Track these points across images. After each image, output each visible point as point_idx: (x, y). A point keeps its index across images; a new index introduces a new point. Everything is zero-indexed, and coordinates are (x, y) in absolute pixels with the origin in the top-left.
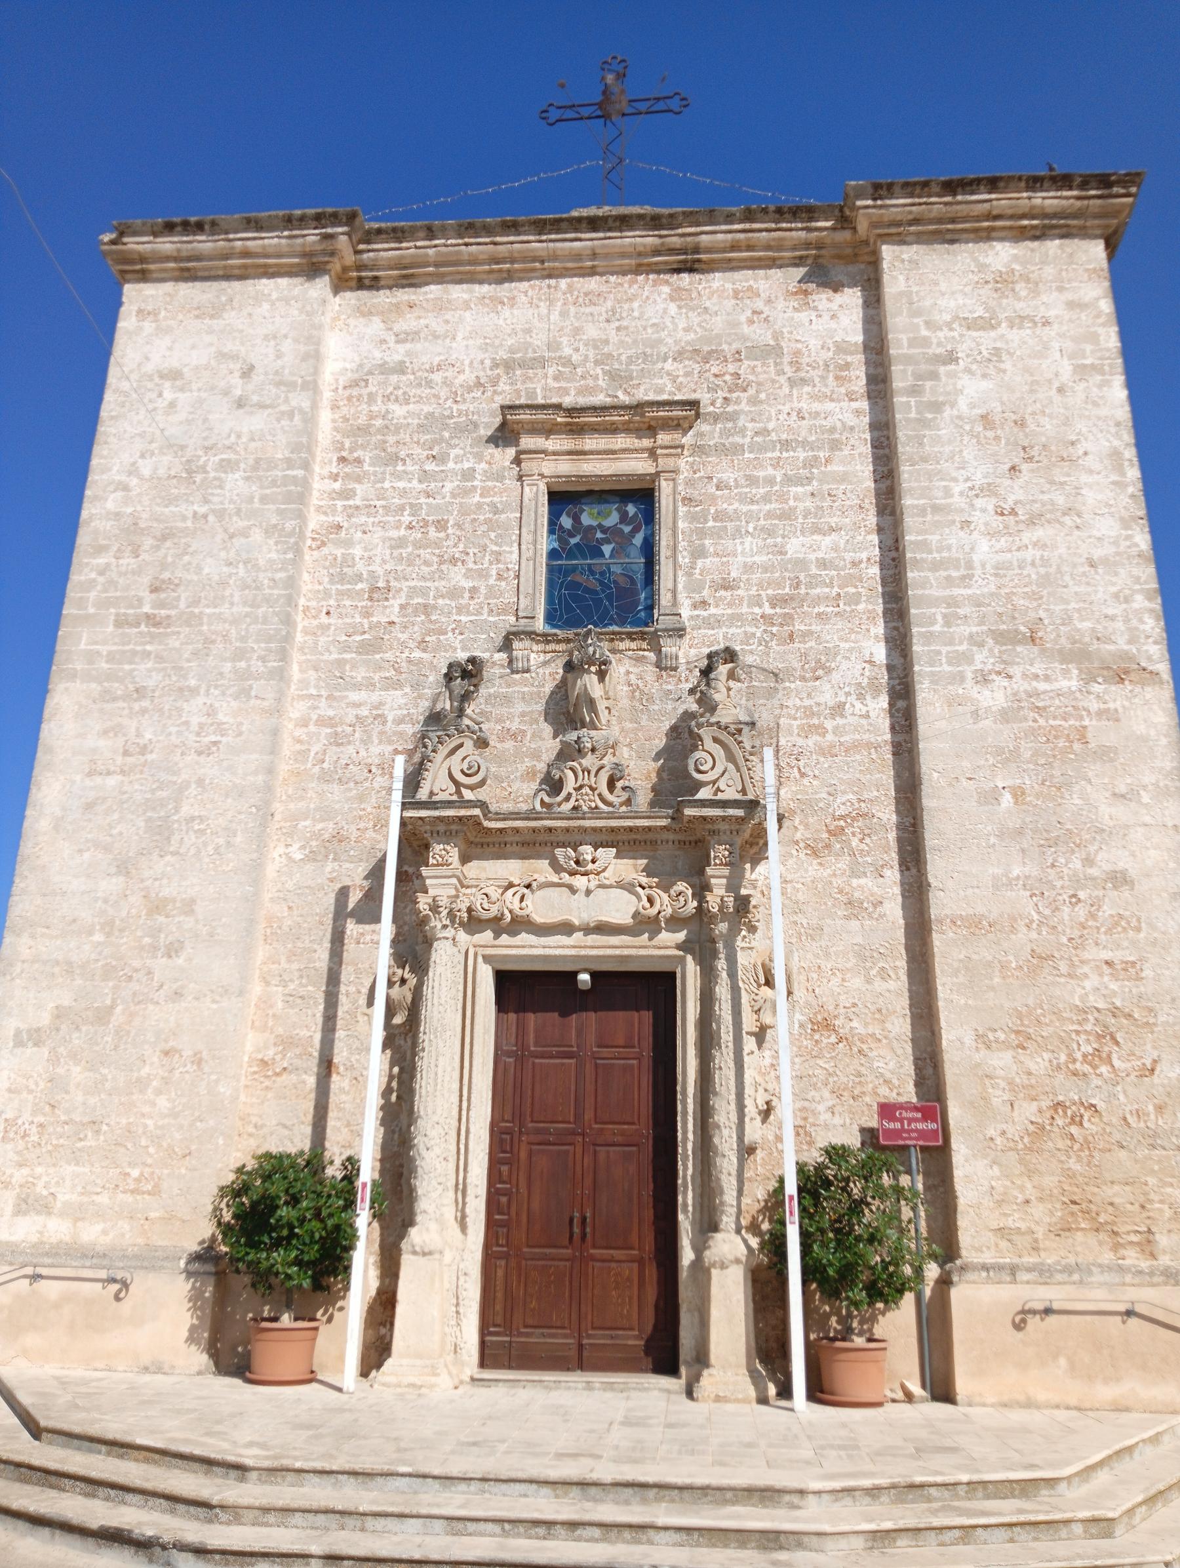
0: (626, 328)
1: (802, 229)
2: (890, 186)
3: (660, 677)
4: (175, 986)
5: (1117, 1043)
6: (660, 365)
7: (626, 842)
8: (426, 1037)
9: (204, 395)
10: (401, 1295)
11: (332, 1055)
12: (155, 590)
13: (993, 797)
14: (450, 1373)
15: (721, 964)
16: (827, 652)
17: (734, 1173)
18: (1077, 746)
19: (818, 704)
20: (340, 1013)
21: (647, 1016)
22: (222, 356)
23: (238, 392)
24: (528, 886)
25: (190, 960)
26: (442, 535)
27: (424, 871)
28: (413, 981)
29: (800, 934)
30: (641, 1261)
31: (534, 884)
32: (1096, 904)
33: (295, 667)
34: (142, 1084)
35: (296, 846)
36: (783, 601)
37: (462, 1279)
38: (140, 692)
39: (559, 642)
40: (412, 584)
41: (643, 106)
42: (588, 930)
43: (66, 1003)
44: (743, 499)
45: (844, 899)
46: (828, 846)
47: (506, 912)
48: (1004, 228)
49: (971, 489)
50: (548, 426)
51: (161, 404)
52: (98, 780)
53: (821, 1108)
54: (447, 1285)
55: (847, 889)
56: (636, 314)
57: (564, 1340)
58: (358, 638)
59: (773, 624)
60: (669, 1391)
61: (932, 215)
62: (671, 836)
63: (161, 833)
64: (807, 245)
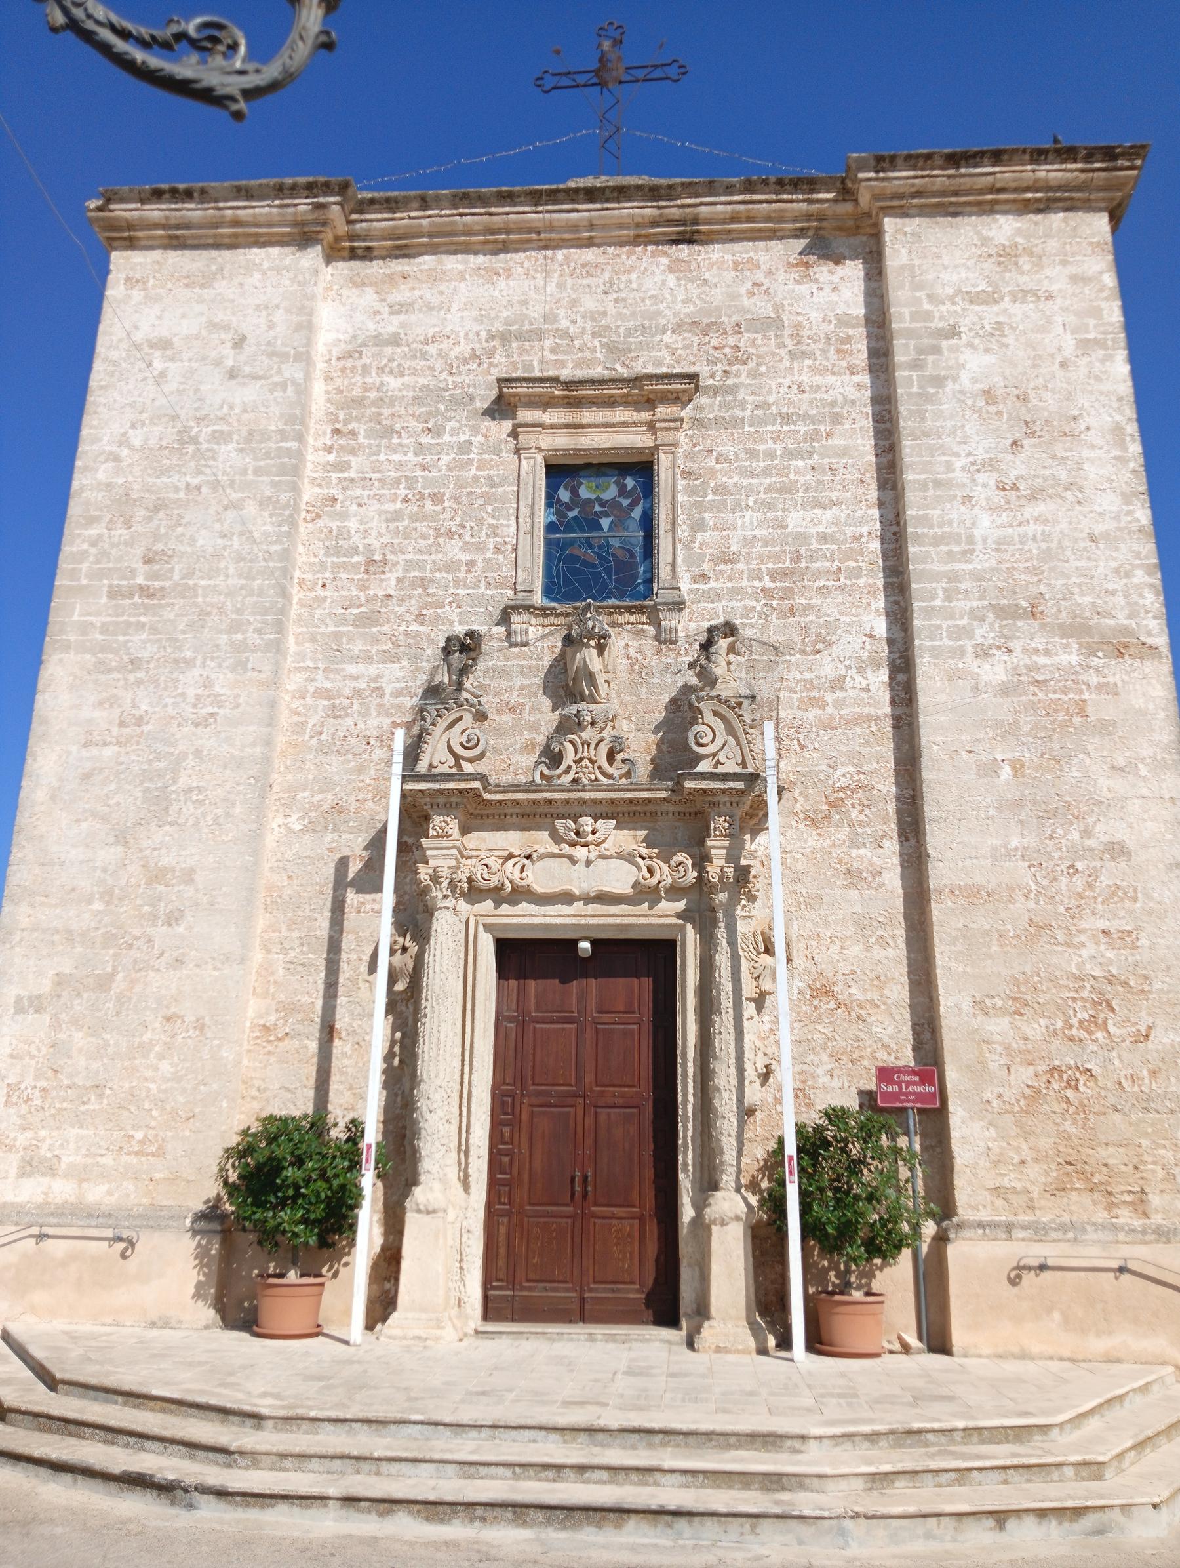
0: (624, 300)
1: (803, 201)
2: (893, 159)
4: (176, 954)
5: (1113, 1010)
6: (658, 338)
8: (428, 1004)
9: (195, 365)
13: (993, 769)
15: (721, 932)
17: (734, 1134)
18: (1076, 720)
19: (819, 678)
20: (341, 980)
21: (647, 983)
22: (213, 326)
24: (529, 857)
26: (439, 508)
27: (425, 843)
28: (414, 949)
30: (641, 1218)
31: (535, 855)
32: (1093, 874)
33: (291, 640)
34: (144, 1049)
37: (465, 1236)
39: (557, 615)
40: (409, 557)
41: (640, 74)
42: (588, 899)
43: (67, 970)
44: (743, 472)
45: (843, 869)
46: (827, 817)
47: (507, 882)
48: (1007, 201)
50: (545, 399)
52: (95, 751)
53: (820, 1071)
54: (450, 1242)
55: (847, 859)
56: (634, 286)
57: (565, 1294)
58: (355, 611)
59: (773, 598)
60: (670, 1342)
61: (935, 188)
62: (671, 808)
63: (159, 804)
64: (808, 217)
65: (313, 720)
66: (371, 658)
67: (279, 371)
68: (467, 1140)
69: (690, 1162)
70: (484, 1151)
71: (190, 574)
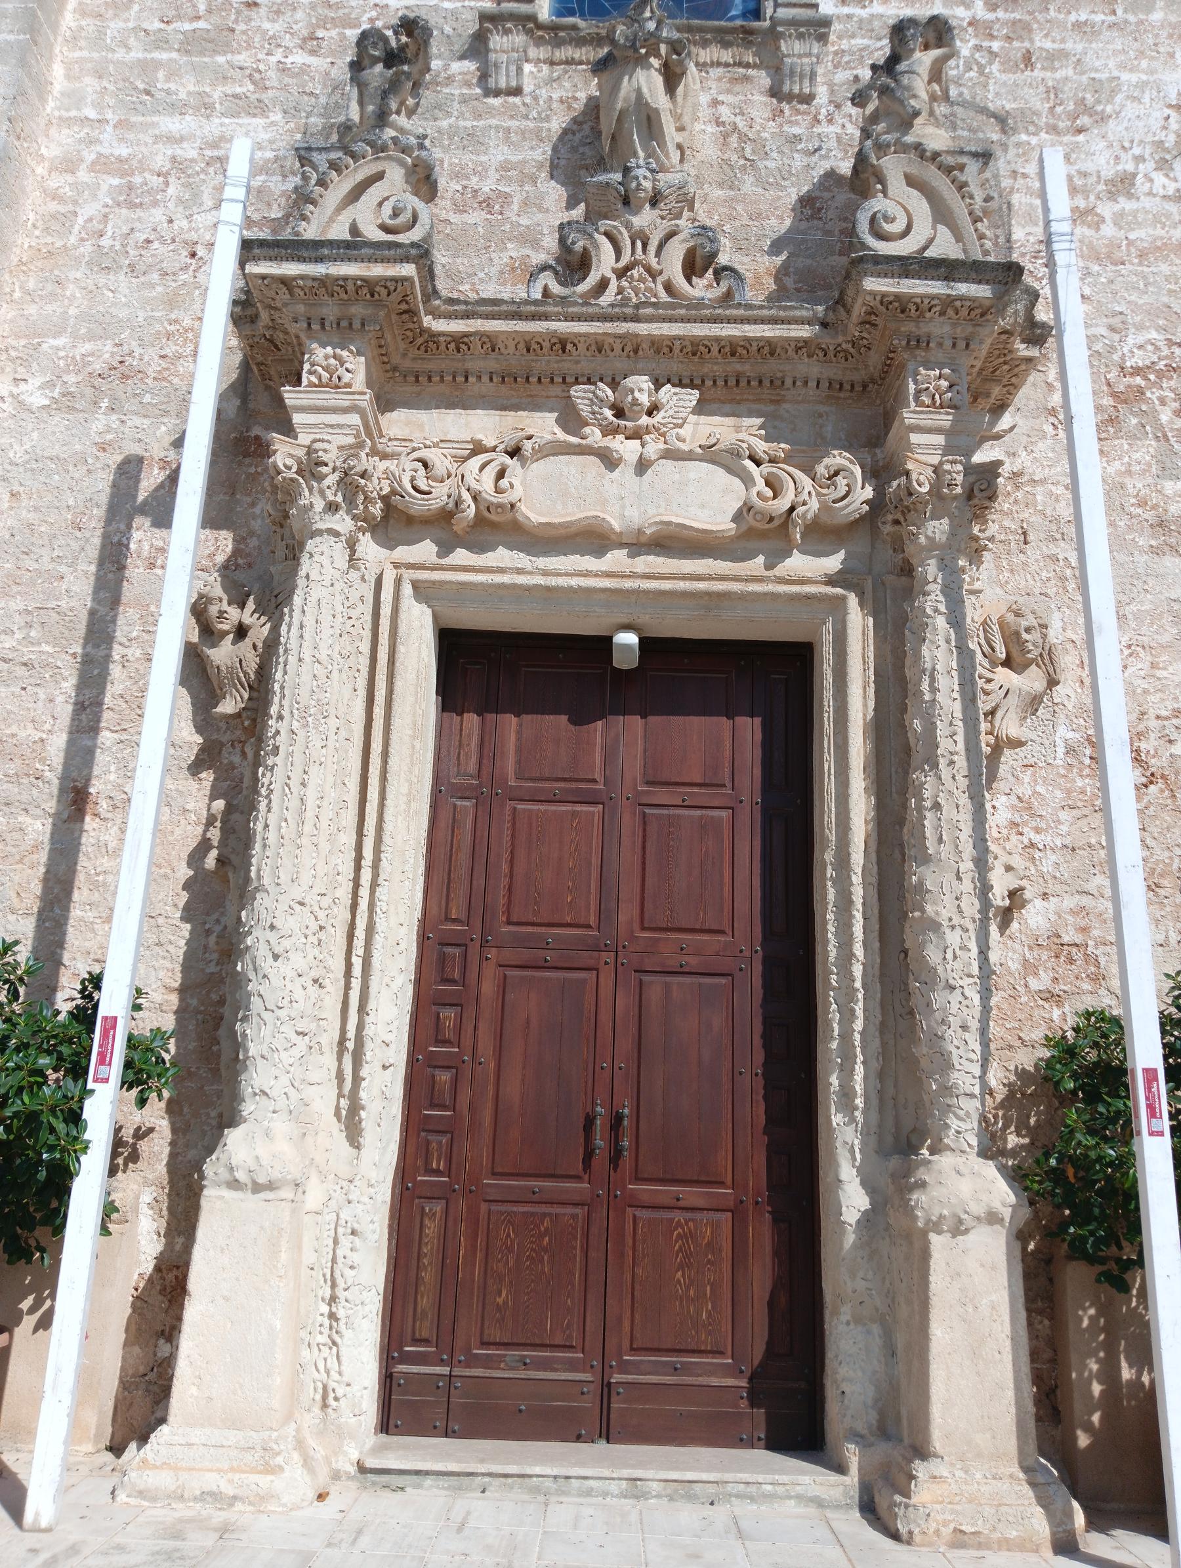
3: (777, 113)
7: (726, 376)
8: (283, 726)
10: (195, 1282)
11: (88, 780)
14: (307, 1463)
15: (934, 600)
16: (1096, 85)
17: (974, 1025)
19: (1084, 175)
20: (108, 700)
21: (750, 728)
24: (514, 452)
27: (290, 396)
28: (260, 631)
29: (1063, 579)
30: (737, 1212)
31: (528, 446)
33: (58, 71)
37: (345, 1242)
39: (580, 42)
42: (639, 544)
45: (1150, 515)
47: (466, 496)
54: (309, 1257)
55: (1154, 499)
57: (569, 1375)
58: (187, 26)
59: (992, 37)
60: (819, 1503)
62: (812, 368)
65: (90, 210)
66: (209, 107)
68: (360, 1027)
69: (859, 1088)
70: (398, 1054)
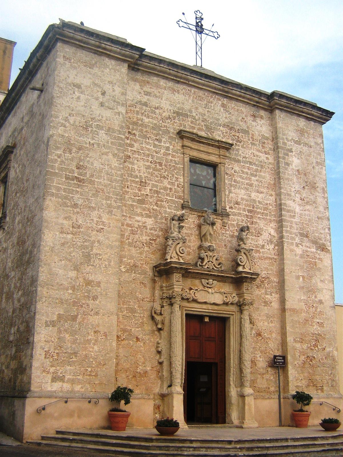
0: (210, 112)
4: (96, 310)
5: (319, 342)
6: (219, 127)
9: (90, 98)
12: (78, 168)
13: (298, 277)
18: (314, 266)
19: (259, 244)
22: (95, 85)
23: (101, 100)
25: (100, 302)
26: (161, 168)
32: (316, 308)
34: (89, 341)
35: (123, 267)
36: (249, 211)
38: (76, 205)
40: (153, 183)
43: (62, 313)
44: (241, 177)
46: (260, 286)
49: (295, 190)
51: (75, 97)
52: (65, 235)
53: (258, 356)
56: (212, 108)
58: (138, 198)
63: (88, 258)
65: (126, 234)
66: (143, 215)
67: (117, 108)
71: (92, 176)
